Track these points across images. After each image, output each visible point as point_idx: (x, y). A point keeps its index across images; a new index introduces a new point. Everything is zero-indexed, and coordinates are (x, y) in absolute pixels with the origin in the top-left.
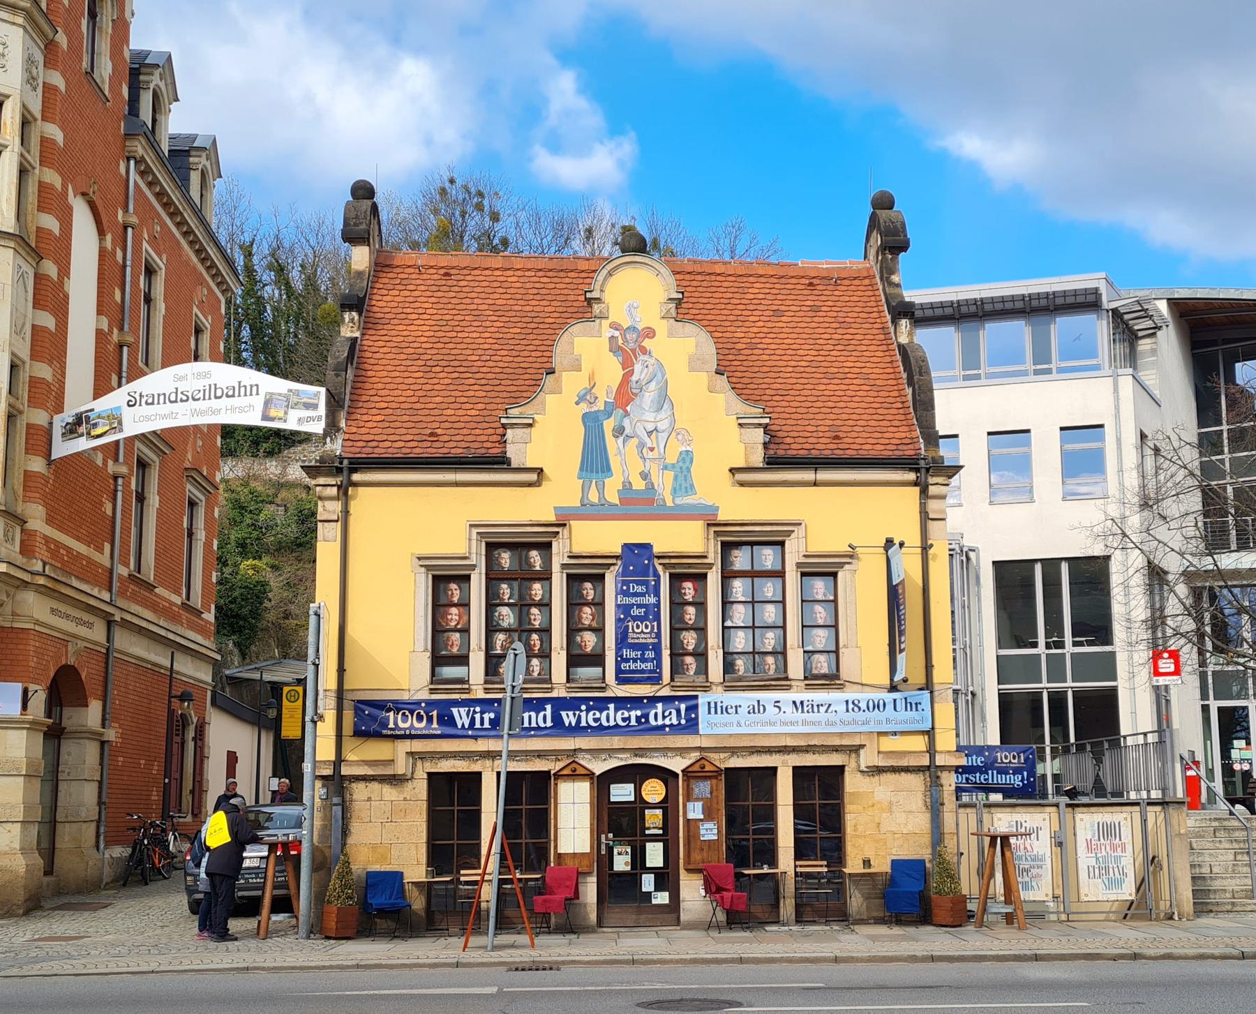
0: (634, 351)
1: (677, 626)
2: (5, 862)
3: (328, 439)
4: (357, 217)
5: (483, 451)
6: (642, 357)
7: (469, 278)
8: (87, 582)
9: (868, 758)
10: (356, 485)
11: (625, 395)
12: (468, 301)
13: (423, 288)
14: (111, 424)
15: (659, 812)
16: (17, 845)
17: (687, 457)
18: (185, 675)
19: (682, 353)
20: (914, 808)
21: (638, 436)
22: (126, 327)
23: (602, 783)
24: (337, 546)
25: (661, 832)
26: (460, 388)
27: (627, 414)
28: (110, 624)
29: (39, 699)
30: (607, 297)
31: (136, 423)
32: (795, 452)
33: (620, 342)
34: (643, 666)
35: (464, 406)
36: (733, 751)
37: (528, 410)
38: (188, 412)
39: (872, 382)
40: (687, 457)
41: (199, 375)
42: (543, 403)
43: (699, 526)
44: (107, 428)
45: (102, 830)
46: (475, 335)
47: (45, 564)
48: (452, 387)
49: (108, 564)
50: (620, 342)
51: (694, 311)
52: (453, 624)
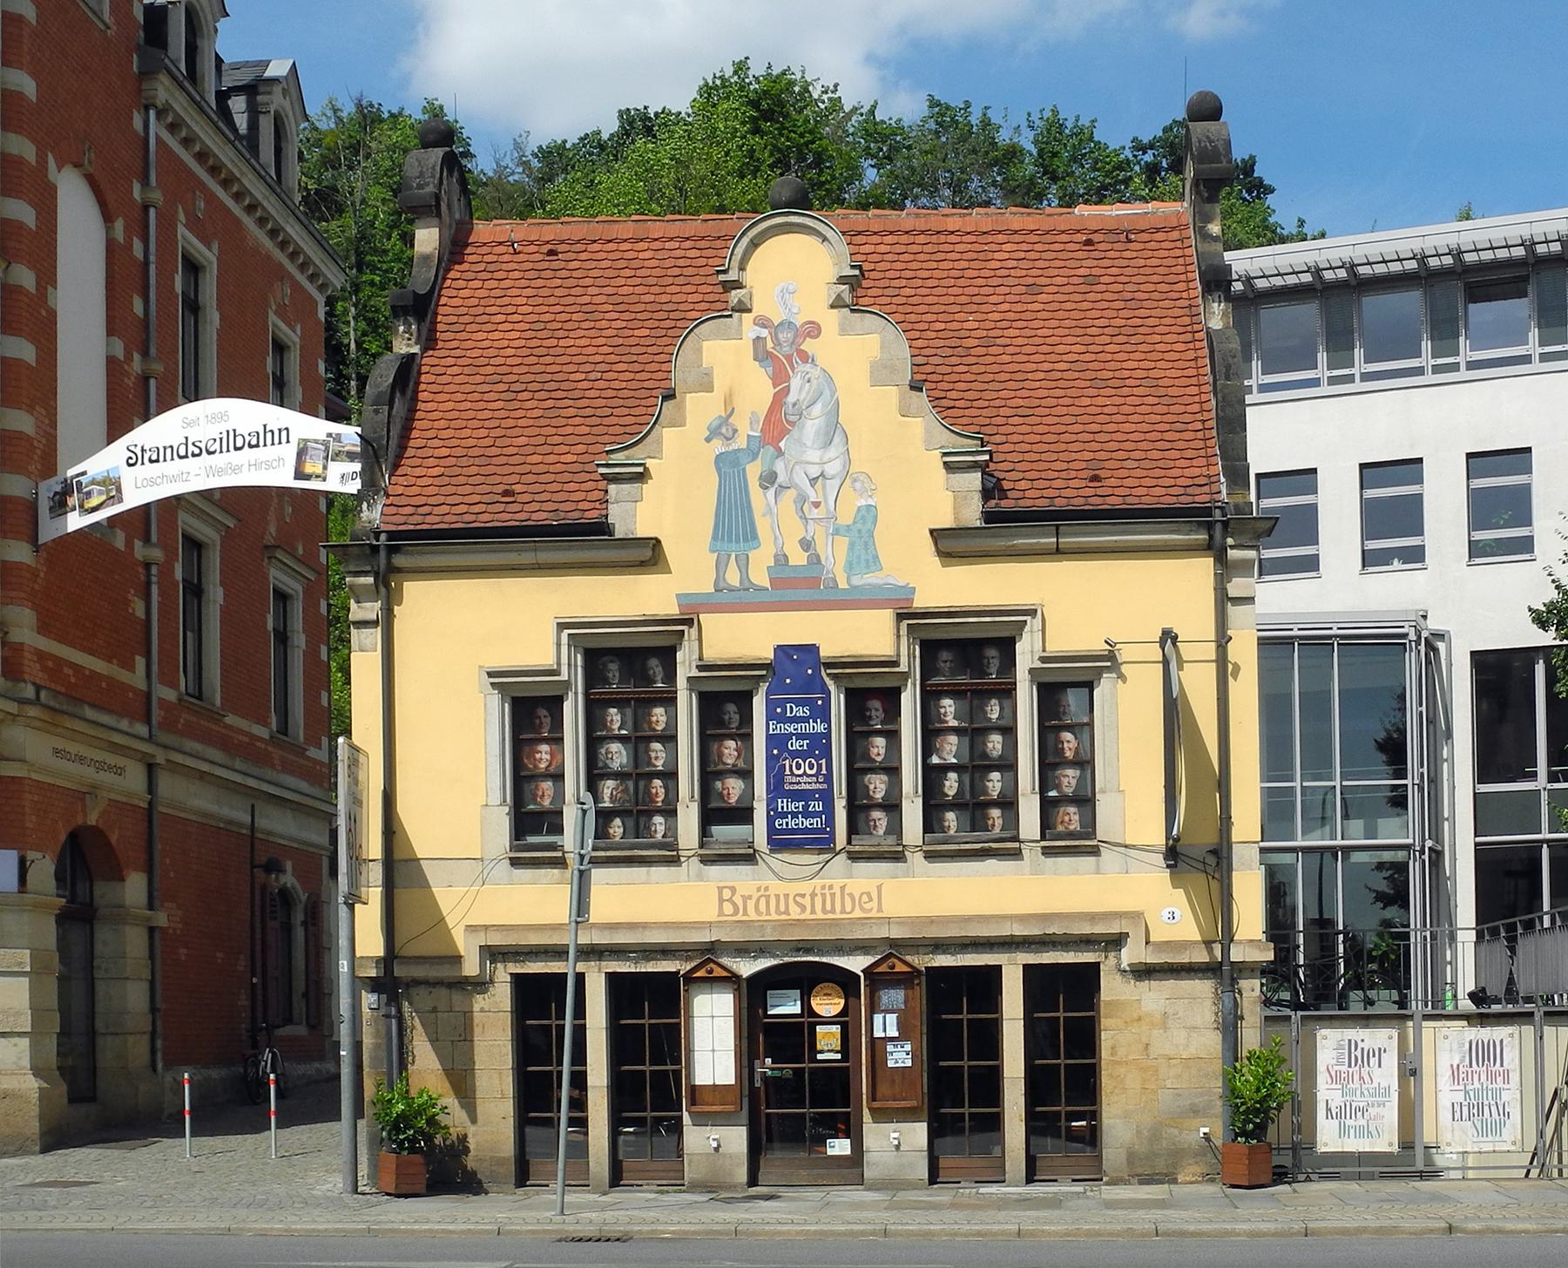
0: (789, 358)
1: (859, 765)
2: (8, 1084)
3: (365, 505)
4: (421, 175)
5: (576, 515)
6: (802, 367)
7: (583, 256)
8: (110, 711)
9: (1130, 954)
10: (399, 570)
11: (777, 424)
12: (578, 291)
13: (517, 275)
14: (108, 491)
15: (836, 1029)
16: (26, 1062)
17: (868, 515)
18: (282, 837)
19: (858, 361)
20: (1199, 1022)
21: (796, 487)
22: (153, 351)
23: (753, 993)
24: (377, 657)
25: (839, 1056)
26: (554, 422)
27: (780, 453)
28: (151, 768)
29: (44, 870)
30: (749, 277)
31: (142, 489)
32: (1029, 503)
33: (770, 345)
34: (806, 823)
35: (556, 449)
36: (939, 946)
37: (637, 454)
38: (203, 472)
39: (1162, 391)
40: (868, 515)
41: (214, 418)
42: (659, 442)
43: (887, 616)
44: (104, 497)
45: (159, 1043)
46: (583, 342)
47: (38, 688)
48: (543, 422)
49: (142, 686)
50: (770, 345)
51: (908, 291)
52: (543, 766)
